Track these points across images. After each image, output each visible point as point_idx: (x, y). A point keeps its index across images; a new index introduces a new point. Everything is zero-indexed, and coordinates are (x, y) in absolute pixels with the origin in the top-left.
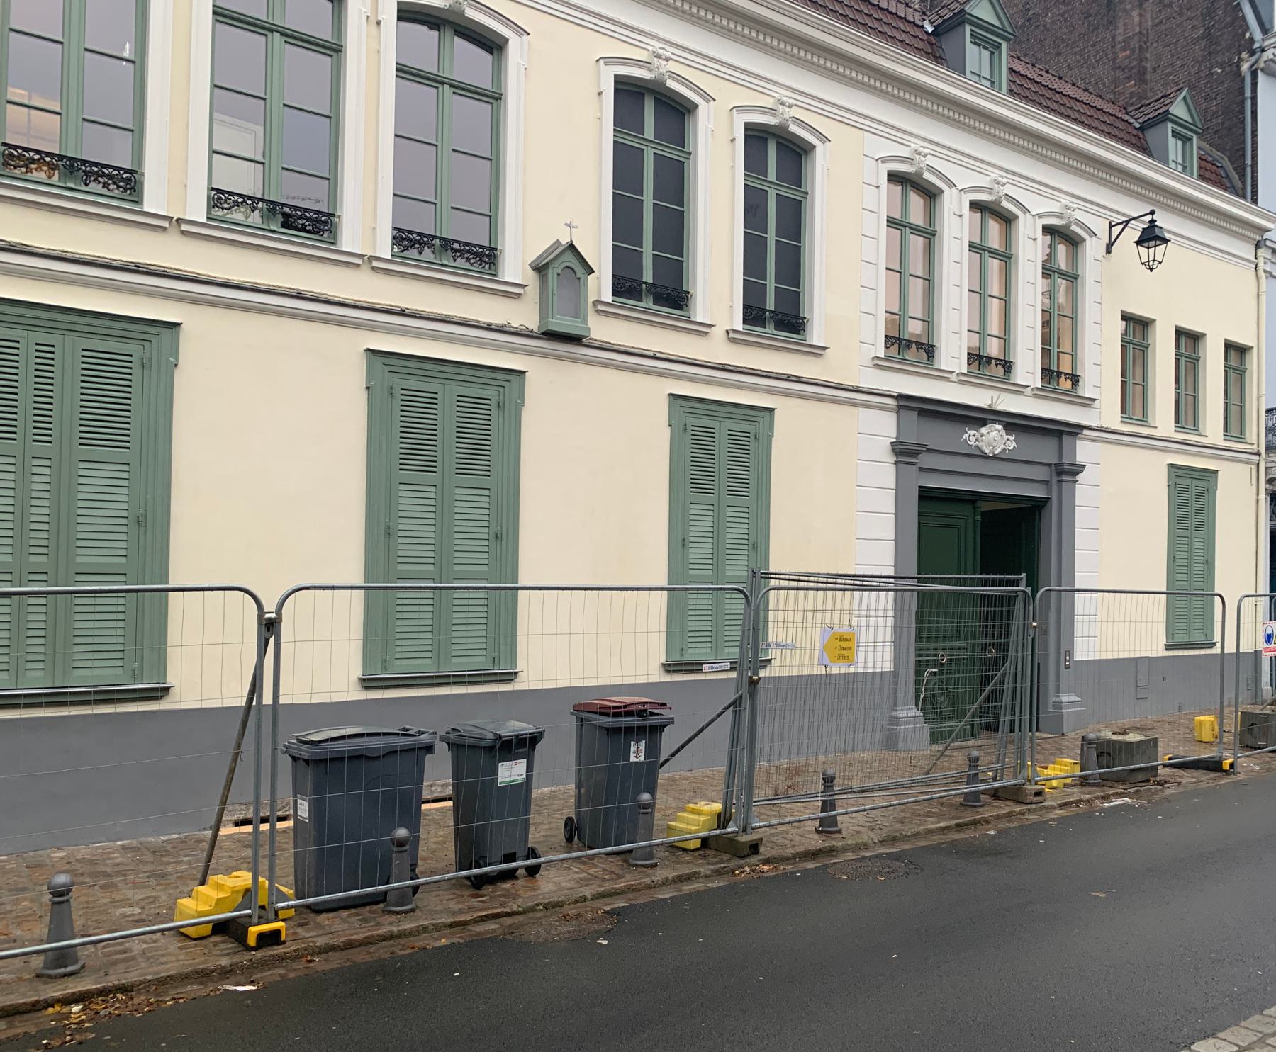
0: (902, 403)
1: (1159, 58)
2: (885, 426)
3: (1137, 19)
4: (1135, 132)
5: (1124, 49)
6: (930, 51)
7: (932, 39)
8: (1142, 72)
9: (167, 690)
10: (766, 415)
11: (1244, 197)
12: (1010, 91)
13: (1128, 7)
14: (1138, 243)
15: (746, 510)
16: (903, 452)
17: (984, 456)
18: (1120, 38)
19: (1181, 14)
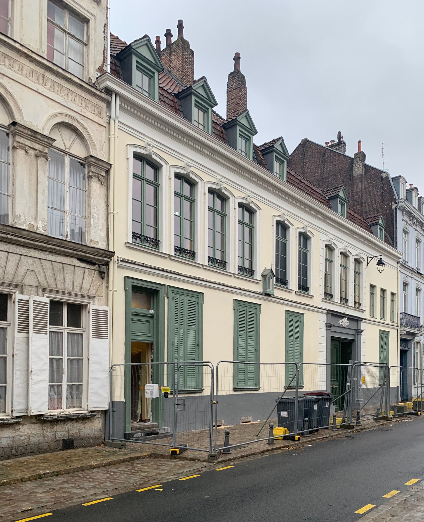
0: (328, 312)
1: (367, 199)
2: (323, 318)
3: (360, 186)
4: (327, 201)
5: (356, 195)
6: (173, 105)
7: (369, 227)
8: (362, 203)
9: (203, 390)
10: (201, 295)
11: (393, 247)
12: (347, 218)
13: (358, 182)
14: (377, 264)
15: (253, 338)
16: (328, 326)
17: (343, 327)
18: (355, 191)
19: (373, 187)
